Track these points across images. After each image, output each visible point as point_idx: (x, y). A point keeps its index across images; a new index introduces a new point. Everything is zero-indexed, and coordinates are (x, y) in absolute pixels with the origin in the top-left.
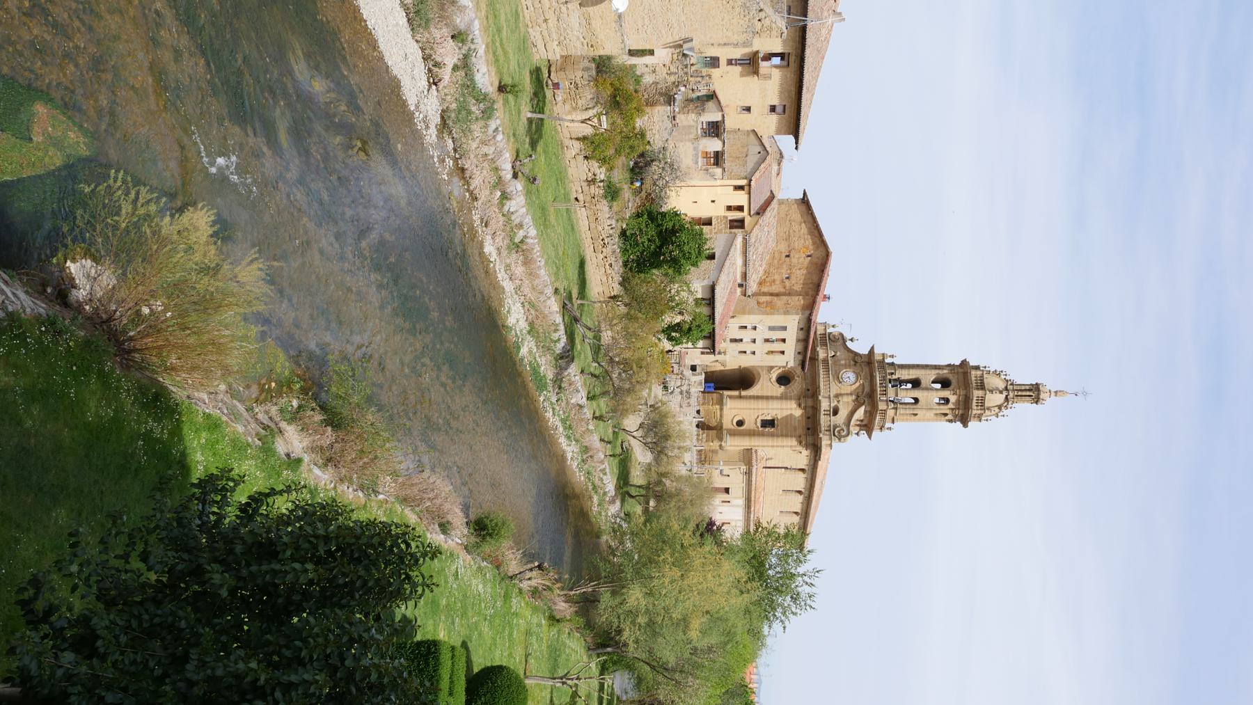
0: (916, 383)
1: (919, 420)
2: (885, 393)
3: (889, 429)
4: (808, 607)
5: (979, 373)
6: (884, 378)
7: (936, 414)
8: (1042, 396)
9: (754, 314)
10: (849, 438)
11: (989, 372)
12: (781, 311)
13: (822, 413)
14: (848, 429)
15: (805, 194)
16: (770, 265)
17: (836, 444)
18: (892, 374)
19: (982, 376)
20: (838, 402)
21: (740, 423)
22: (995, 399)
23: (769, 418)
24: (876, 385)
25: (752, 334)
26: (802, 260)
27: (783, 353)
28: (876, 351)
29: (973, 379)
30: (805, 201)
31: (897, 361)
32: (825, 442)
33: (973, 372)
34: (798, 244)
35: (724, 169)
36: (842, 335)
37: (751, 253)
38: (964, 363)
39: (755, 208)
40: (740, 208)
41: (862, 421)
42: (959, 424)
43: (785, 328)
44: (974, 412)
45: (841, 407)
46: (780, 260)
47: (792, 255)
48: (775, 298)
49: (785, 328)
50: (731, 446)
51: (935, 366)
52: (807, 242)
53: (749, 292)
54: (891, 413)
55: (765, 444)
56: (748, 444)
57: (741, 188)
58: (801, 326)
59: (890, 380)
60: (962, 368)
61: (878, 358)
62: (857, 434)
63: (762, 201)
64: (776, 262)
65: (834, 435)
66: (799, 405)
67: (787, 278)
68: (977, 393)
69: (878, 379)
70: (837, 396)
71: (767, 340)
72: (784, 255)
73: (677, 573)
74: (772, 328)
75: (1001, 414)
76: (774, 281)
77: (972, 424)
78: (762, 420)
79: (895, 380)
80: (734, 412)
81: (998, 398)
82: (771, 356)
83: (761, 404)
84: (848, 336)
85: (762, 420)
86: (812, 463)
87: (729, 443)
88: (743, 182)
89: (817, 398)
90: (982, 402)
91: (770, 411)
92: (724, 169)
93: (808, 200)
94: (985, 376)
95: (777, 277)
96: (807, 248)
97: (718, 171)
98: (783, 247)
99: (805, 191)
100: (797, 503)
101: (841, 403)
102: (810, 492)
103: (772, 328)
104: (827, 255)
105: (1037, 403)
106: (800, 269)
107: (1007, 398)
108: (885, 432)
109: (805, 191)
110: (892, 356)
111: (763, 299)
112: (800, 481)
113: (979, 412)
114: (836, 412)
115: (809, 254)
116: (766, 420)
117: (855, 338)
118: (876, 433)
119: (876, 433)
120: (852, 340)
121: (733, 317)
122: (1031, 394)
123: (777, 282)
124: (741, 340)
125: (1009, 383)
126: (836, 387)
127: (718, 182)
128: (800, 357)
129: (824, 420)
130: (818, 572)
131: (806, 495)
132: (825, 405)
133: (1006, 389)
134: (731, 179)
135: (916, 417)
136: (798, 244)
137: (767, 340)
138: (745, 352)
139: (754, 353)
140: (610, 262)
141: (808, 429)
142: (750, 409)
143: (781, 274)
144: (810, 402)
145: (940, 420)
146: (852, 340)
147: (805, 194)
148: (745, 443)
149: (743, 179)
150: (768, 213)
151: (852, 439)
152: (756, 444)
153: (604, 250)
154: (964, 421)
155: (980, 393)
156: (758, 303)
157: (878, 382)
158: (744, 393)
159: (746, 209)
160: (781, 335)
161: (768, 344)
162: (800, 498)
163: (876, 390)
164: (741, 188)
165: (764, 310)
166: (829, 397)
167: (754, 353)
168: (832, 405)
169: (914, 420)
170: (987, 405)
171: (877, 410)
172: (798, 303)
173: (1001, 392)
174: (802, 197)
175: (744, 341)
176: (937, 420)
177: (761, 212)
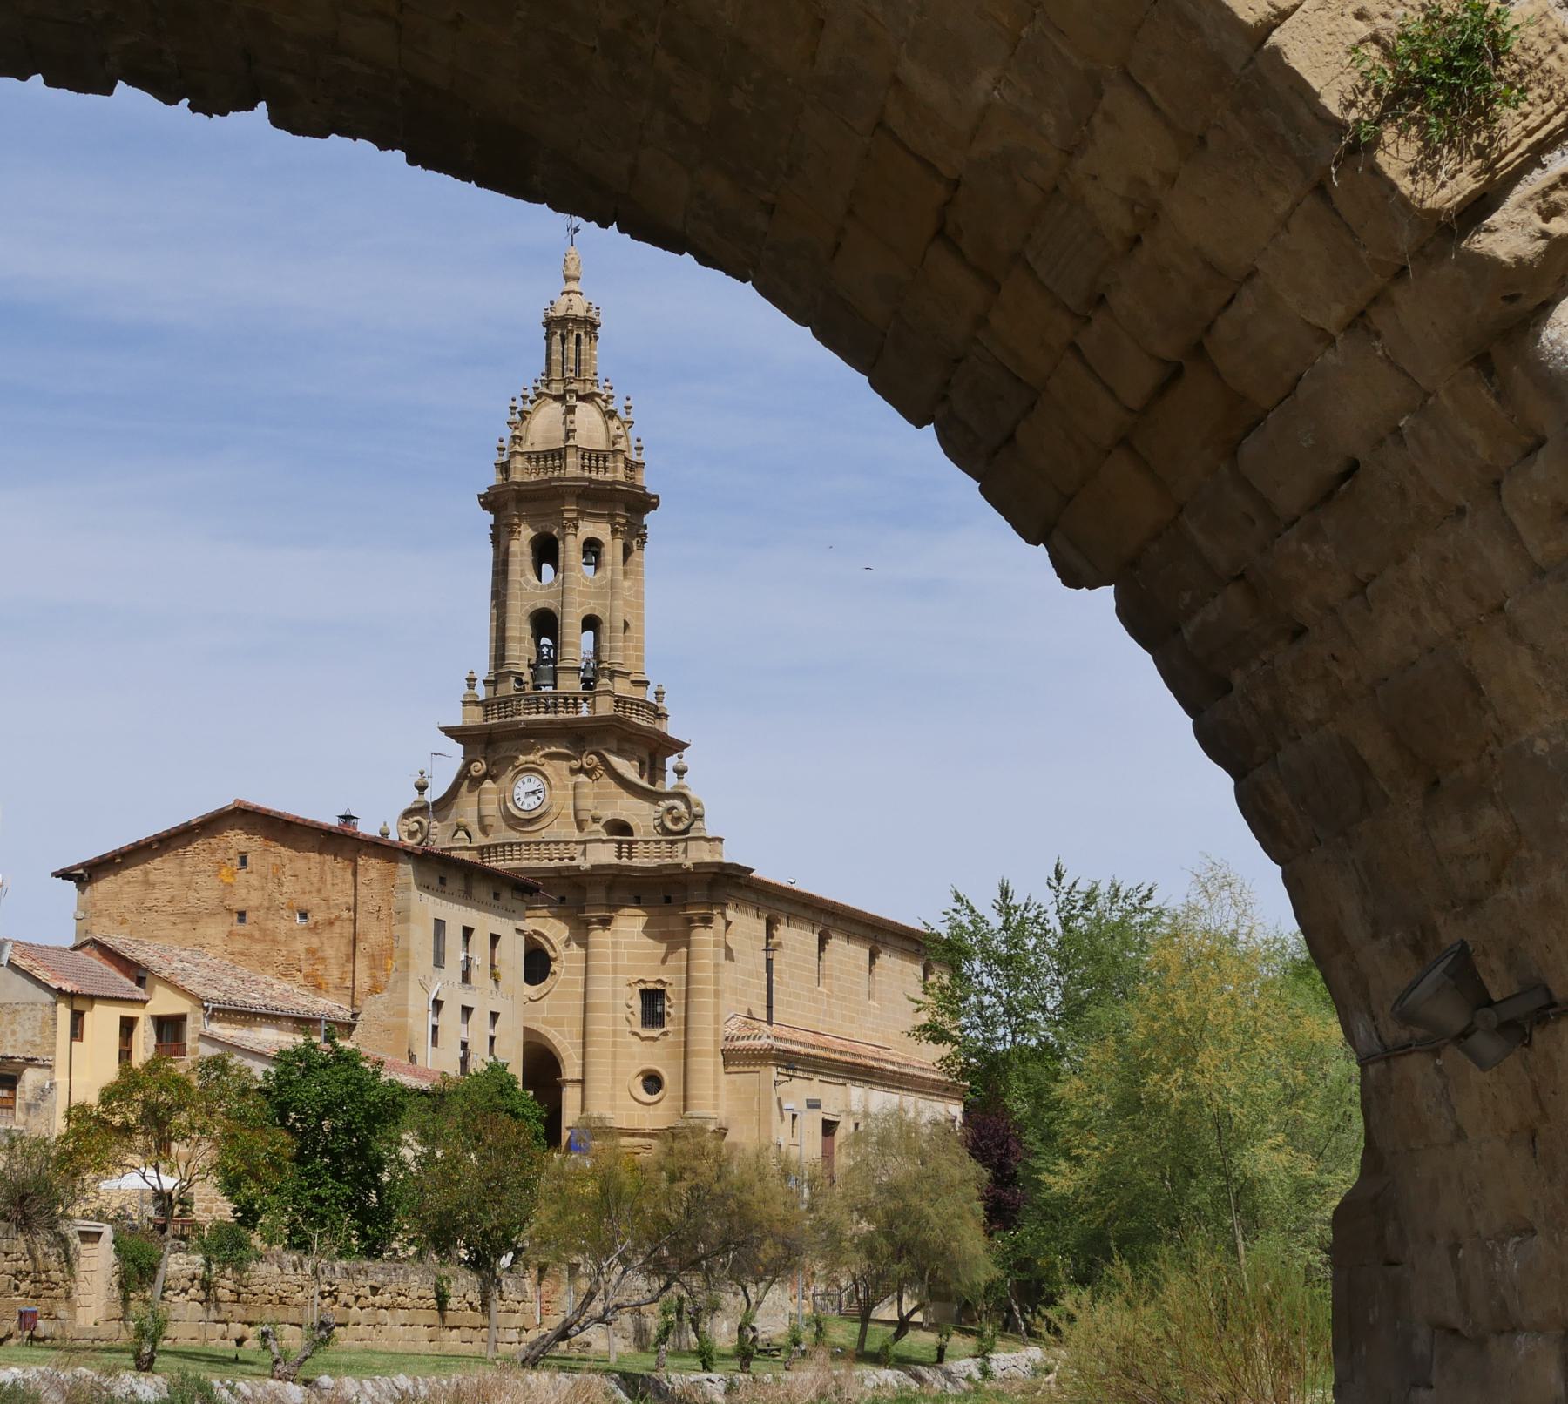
0: (545, 623)
1: (640, 618)
2: (572, 701)
3: (659, 694)
4: (1148, 905)
5: (519, 463)
6: (534, 703)
7: (625, 573)
8: (580, 312)
9: (406, 999)
10: (692, 794)
11: (516, 439)
12: (398, 930)
13: (625, 861)
14: (669, 796)
15: (65, 875)
16: (264, 963)
17: (709, 827)
18: (519, 681)
19: (528, 456)
20: (596, 820)
21: (652, 1082)
22: (589, 425)
23: (637, 1004)
24: (551, 722)
25: (451, 1013)
26: (254, 880)
27: (495, 938)
28: (457, 721)
29: (533, 478)
30: (85, 875)
31: (483, 670)
32: (698, 854)
33: (517, 476)
34: (208, 890)
35: (30, 1062)
36: (408, 814)
37: (249, 1001)
38: (490, 501)
39: (126, 985)
40: (128, 1025)
41: (642, 764)
42: (649, 519)
43: (440, 925)
44: (621, 477)
45: (607, 815)
46: (251, 937)
47: (239, 906)
48: (361, 946)
49: (440, 925)
50: (716, 1107)
51: (495, 573)
52: (201, 867)
53: (344, 1015)
54: (622, 687)
55: (710, 1014)
56: (711, 1060)
57: (77, 1018)
58: (435, 882)
59: (537, 687)
60: (505, 506)
61: (476, 717)
62: (680, 772)
63: (112, 971)
64: (257, 948)
65: (686, 831)
66: (605, 923)
67: (304, 915)
68: (573, 467)
69: (533, 717)
70: (580, 825)
71: (466, 978)
72: (239, 928)
73: (1207, 1057)
74: (439, 962)
75: (622, 413)
76: (311, 951)
77: (648, 481)
78: (645, 1024)
79: (534, 677)
80: (624, 1099)
81: (587, 416)
82: (502, 970)
83: (601, 1025)
84: (410, 798)
85: (645, 1024)
86: (753, 897)
87: (710, 1113)
88: (64, 1013)
89: (587, 874)
90: (592, 457)
91: (621, 1002)
92: (30, 1062)
93: (82, 866)
94: (526, 448)
95: (300, 946)
96: (220, 865)
97: (31, 1077)
98: (215, 930)
99: (56, 875)
100: (847, 953)
101: (599, 813)
102: (822, 911)
103: (439, 962)
104: (245, 817)
105: (595, 326)
106: (280, 884)
107: (587, 398)
108: (666, 705)
109: (56, 875)
110: (471, 682)
111: (363, 979)
112: (796, 938)
113: (621, 465)
114: (620, 828)
115: (237, 861)
116: (644, 1013)
117: (417, 778)
118: (672, 728)
119: (672, 729)
120: (421, 788)
121: (412, 1058)
122: (573, 339)
123: (315, 941)
124: (464, 1045)
125: (543, 389)
126: (555, 827)
127: (61, 1078)
128: (506, 895)
129: (644, 859)
130: (1059, 876)
131: (830, 921)
132: (604, 854)
133: (560, 398)
134: (54, 1044)
135: (632, 625)
136: (208, 890)
137: (466, 978)
138: (492, 1039)
139: (494, 1016)
140: (367, 1291)
141: (668, 900)
142: (614, 1055)
143: (291, 936)
144: (598, 895)
145: (640, 564)
146: (421, 788)
147: (65, 875)
148: (707, 1065)
149: (55, 1012)
150: (140, 955)
151: (694, 786)
152: (711, 1039)
153: (343, 1297)
154: (642, 503)
155: (573, 460)
156: (375, 989)
157: (542, 716)
158: (571, 1071)
159: (129, 1012)
160: (453, 936)
161: (474, 974)
162: (837, 943)
163: (564, 721)
164: (77, 1018)
165: (393, 976)
166: (585, 842)
167: (494, 1016)
168: (605, 837)
169: (640, 629)
170: (601, 444)
171: (618, 719)
172: (376, 886)
173: (571, 410)
174: (72, 884)
175: (464, 1036)
176: (639, 573)
177: (139, 973)
